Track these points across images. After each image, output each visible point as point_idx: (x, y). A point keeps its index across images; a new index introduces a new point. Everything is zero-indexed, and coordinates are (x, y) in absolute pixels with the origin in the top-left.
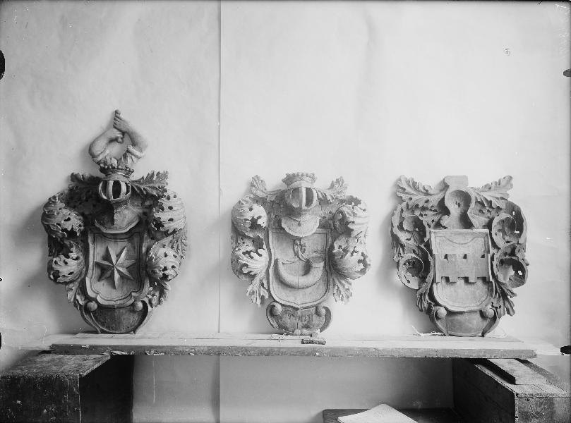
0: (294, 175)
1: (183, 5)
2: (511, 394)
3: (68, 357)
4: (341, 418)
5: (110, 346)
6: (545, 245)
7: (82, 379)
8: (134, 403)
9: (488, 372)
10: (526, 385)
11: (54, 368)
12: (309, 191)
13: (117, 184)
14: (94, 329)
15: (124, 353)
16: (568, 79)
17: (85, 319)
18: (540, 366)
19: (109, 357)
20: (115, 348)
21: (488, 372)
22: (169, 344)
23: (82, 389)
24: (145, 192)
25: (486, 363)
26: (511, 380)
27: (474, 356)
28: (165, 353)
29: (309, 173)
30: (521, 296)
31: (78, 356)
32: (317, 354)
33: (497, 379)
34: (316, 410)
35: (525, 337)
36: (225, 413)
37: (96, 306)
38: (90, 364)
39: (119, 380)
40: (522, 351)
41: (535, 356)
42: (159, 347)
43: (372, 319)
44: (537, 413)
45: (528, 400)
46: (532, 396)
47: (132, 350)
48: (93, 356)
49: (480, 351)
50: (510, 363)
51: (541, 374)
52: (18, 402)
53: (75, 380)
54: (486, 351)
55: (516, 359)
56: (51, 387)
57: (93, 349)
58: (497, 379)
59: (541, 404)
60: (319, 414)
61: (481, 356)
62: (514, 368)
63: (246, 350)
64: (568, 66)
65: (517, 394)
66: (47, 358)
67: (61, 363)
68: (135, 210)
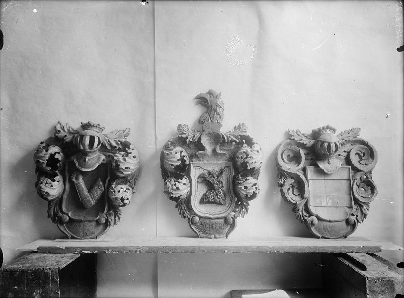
0: (320, 130)
1: (171, 4)
2: (363, 280)
3: (51, 255)
4: (243, 296)
5: (80, 247)
6: (385, 172)
7: (61, 271)
8: (97, 287)
9: (347, 263)
10: (373, 271)
11: (41, 263)
12: (92, 139)
13: (92, 139)
14: (65, 235)
15: (90, 252)
16: (401, 54)
17: (59, 228)
18: (384, 258)
19: (79, 255)
20: (84, 248)
21: (347, 263)
22: (122, 245)
23: (61, 278)
24: (119, 142)
25: (345, 256)
26: (364, 268)
27: (337, 251)
28: (119, 252)
29: (325, 125)
30: (375, 207)
31: (58, 255)
32: (226, 251)
33: (356, 269)
34: (225, 291)
35: (372, 236)
36: (162, 292)
37: (68, 218)
38: (66, 260)
39: (87, 271)
40: (371, 248)
41: (380, 251)
42: (115, 248)
43: (259, 228)
44: (382, 291)
45: (375, 282)
46: (378, 279)
47: (96, 250)
48: (68, 255)
49: (341, 248)
50: (362, 256)
51: (385, 264)
52: (16, 287)
53: (55, 270)
54: (346, 248)
55: (368, 253)
56: (39, 277)
57: (68, 250)
58: (356, 269)
59: (385, 285)
60: (228, 293)
61: (342, 251)
62: (365, 259)
63: (176, 249)
64: (400, 43)
65: (368, 278)
66: (36, 256)
67: (45, 259)
68: (220, 162)
